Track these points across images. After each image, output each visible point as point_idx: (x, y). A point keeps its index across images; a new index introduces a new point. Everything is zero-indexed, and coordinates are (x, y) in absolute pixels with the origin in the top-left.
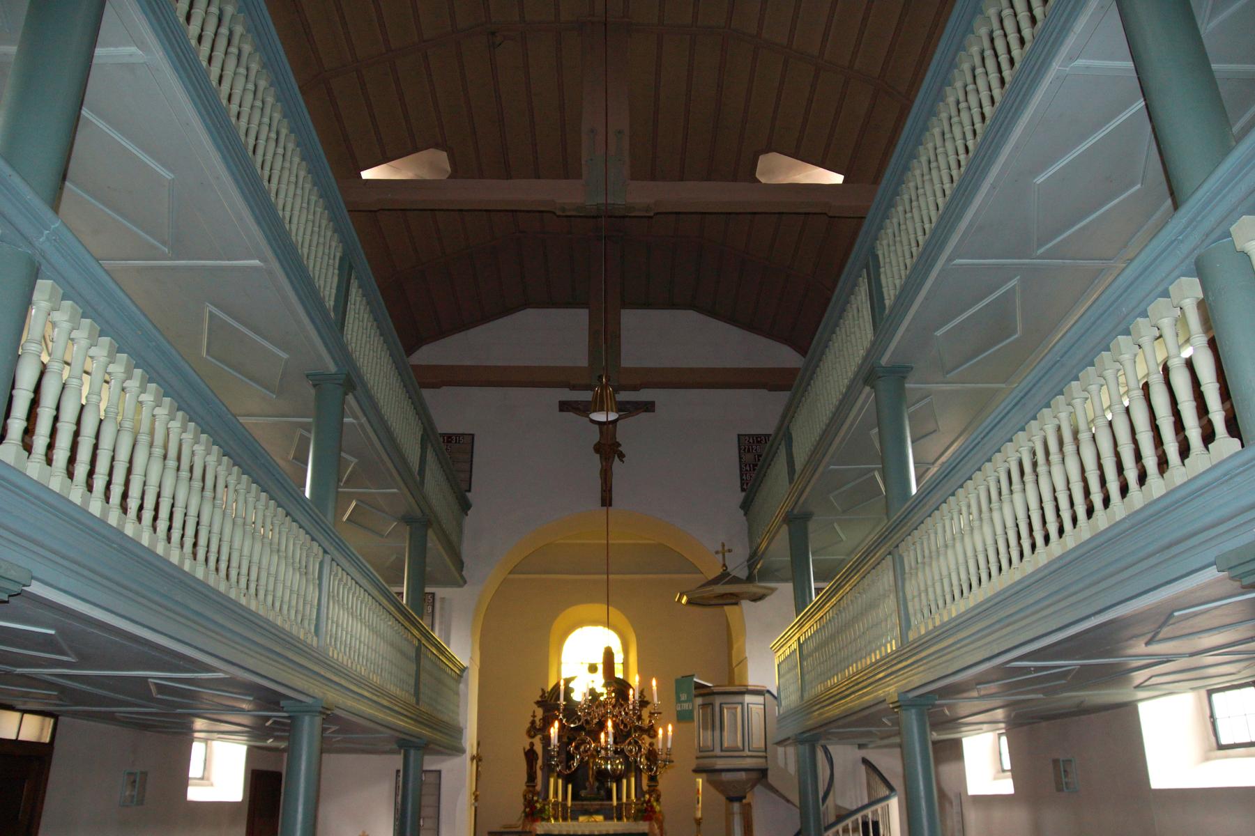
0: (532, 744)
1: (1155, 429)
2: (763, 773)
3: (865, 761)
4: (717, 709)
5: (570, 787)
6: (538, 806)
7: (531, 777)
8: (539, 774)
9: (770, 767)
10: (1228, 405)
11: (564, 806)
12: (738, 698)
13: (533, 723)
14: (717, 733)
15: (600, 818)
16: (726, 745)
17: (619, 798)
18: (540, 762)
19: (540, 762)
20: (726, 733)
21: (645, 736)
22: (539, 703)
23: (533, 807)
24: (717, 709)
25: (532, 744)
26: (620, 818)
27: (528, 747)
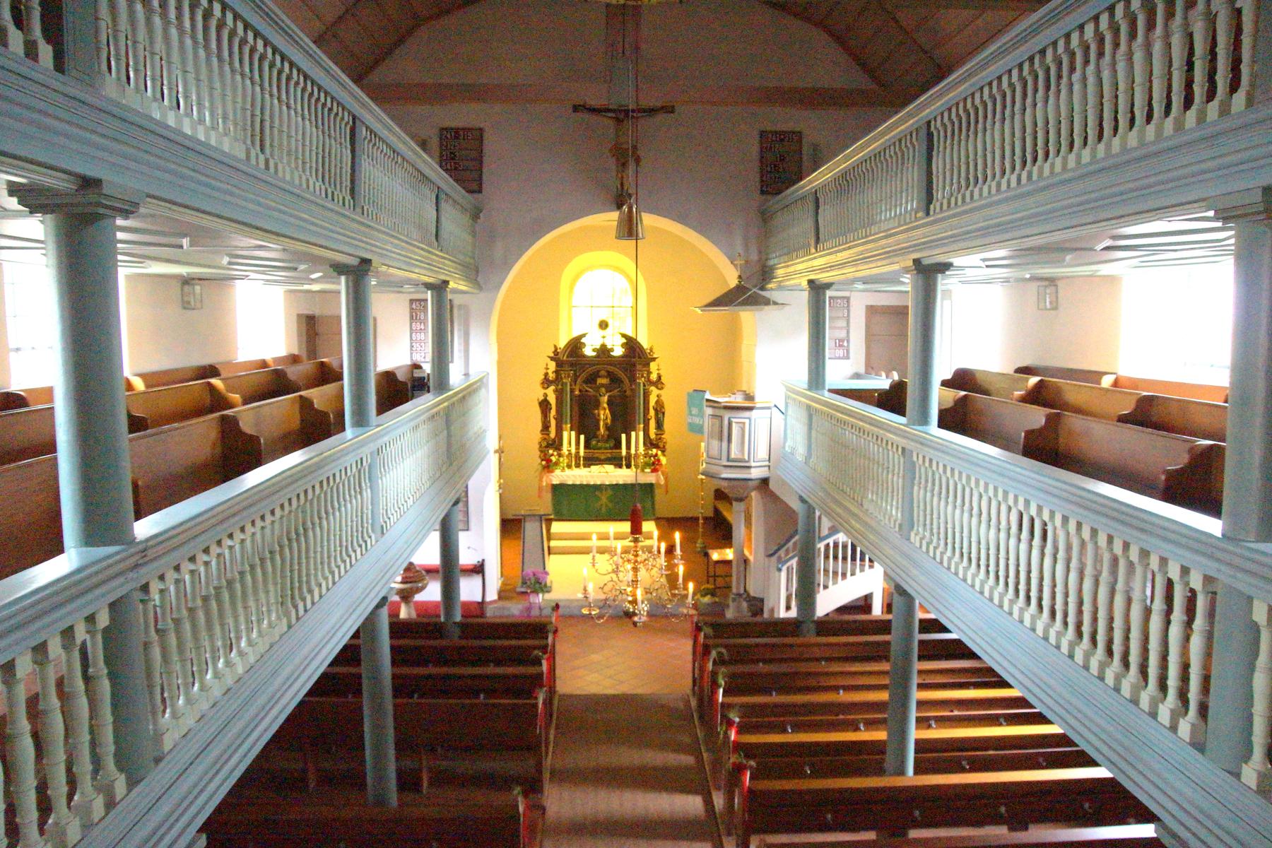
0: (546, 395)
1: (1018, 572)
2: (765, 481)
4: (726, 422)
5: (582, 437)
6: (554, 459)
7: (546, 427)
8: (553, 423)
9: (757, 195)
10: (1002, 720)
11: (577, 456)
12: (746, 414)
13: (546, 374)
14: (725, 444)
15: (610, 468)
16: (733, 456)
17: (628, 447)
18: (553, 412)
19: (553, 412)
20: (733, 445)
21: (653, 388)
22: (552, 359)
23: (549, 461)
24: (726, 422)
25: (546, 395)
26: (628, 466)
27: (542, 398)
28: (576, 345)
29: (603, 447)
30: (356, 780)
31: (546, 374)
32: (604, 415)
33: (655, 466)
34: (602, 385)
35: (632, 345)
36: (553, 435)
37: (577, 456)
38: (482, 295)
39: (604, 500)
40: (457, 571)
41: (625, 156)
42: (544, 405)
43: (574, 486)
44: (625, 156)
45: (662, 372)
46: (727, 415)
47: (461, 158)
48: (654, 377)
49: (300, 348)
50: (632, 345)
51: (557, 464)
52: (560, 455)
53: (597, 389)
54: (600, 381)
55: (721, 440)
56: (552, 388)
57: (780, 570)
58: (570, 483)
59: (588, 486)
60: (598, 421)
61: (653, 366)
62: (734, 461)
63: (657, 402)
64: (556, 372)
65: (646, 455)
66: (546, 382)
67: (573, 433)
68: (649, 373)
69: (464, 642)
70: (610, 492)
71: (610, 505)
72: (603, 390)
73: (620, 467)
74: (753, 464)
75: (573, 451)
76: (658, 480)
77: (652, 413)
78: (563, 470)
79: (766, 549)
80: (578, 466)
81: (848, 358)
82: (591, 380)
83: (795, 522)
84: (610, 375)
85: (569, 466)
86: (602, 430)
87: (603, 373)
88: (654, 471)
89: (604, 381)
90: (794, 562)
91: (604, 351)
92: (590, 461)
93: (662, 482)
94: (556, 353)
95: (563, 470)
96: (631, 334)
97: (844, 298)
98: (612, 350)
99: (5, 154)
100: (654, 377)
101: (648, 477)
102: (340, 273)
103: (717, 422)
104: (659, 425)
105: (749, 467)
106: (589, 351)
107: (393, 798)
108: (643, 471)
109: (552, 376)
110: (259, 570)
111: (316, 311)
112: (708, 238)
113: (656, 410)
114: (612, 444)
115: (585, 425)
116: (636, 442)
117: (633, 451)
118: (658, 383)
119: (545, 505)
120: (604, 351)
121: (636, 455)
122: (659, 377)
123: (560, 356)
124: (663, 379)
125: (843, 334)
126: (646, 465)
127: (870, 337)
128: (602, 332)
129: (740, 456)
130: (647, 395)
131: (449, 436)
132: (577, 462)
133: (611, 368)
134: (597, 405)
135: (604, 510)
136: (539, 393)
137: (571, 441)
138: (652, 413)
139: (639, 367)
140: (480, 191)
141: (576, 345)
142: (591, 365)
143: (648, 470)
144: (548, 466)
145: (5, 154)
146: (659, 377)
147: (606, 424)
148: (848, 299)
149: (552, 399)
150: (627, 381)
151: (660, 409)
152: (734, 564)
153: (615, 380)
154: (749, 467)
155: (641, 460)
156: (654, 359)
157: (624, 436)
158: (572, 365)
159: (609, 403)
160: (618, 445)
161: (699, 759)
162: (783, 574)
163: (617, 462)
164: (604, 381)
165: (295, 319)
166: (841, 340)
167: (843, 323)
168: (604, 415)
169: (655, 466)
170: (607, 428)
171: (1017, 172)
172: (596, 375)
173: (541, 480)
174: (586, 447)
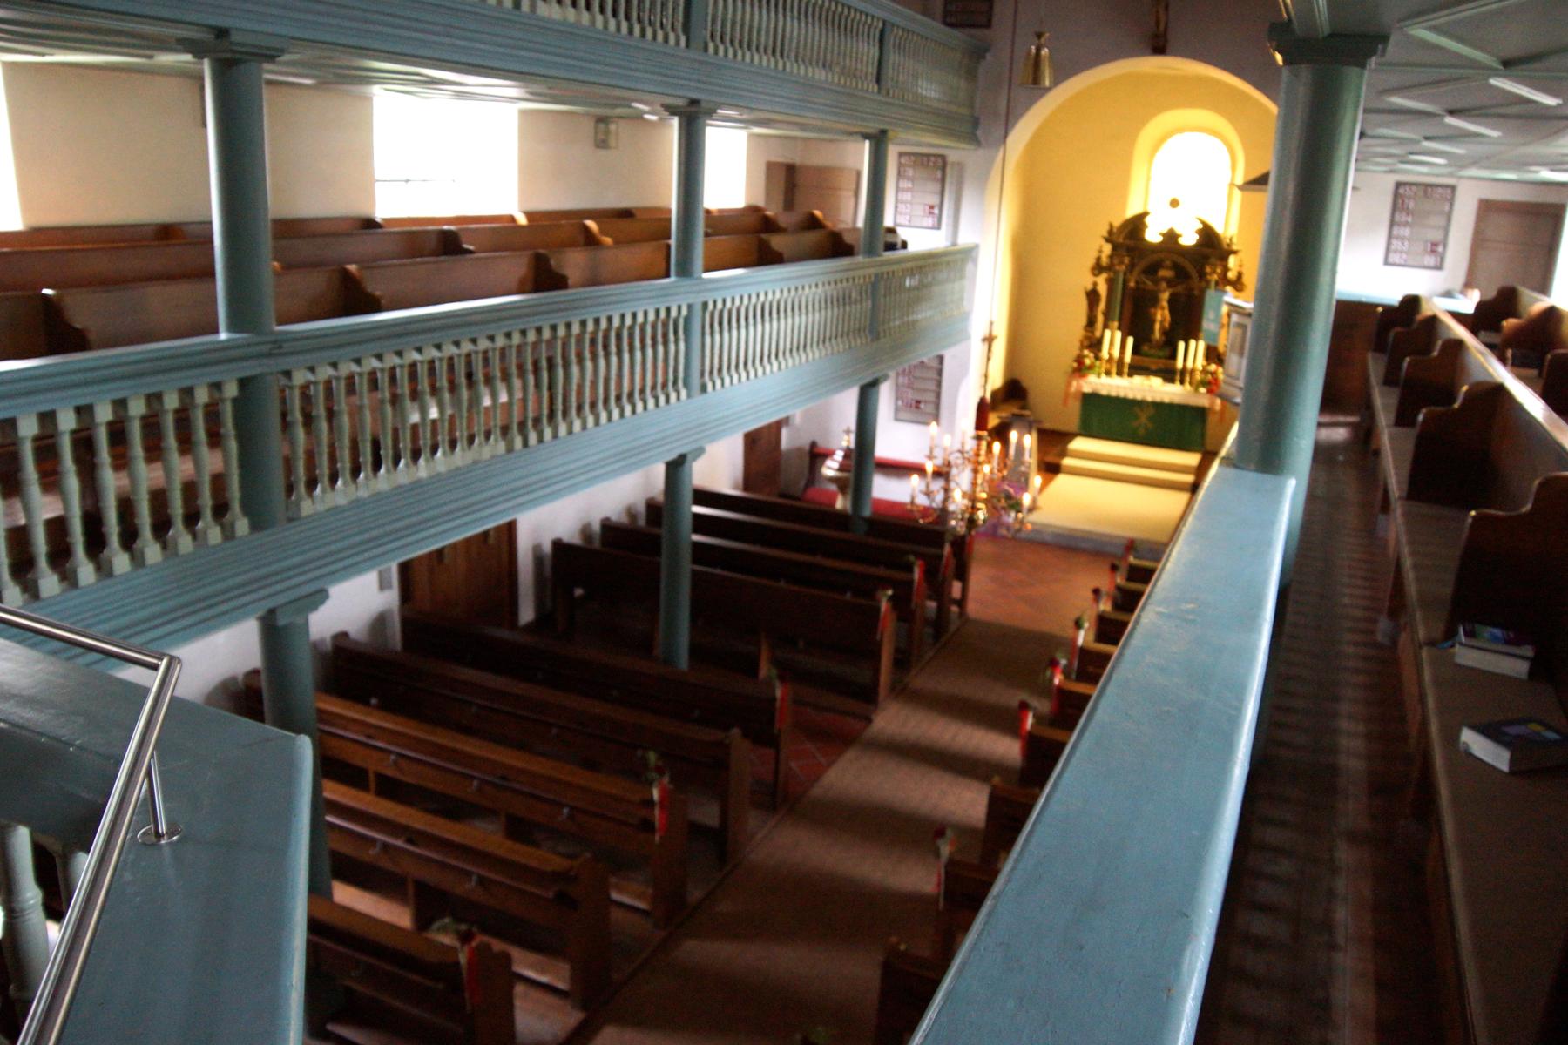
0: (1095, 284)
5: (1130, 341)
6: (1087, 362)
7: (1091, 323)
13: (1098, 259)
18: (1102, 306)
19: (1102, 306)
22: (1108, 240)
25: (1095, 284)
27: (1090, 287)
28: (1136, 225)
29: (1154, 356)
30: (645, 645)
32: (1162, 316)
34: (1164, 279)
35: (1208, 236)
38: (981, 152)
39: (1143, 419)
40: (871, 466)
42: (1092, 296)
49: (768, 195)
50: (1208, 236)
51: (1091, 368)
52: (1097, 358)
53: (1156, 282)
56: (1104, 276)
60: (1153, 322)
61: (1232, 261)
64: (1111, 257)
65: (1205, 371)
66: (1098, 268)
67: (1118, 335)
68: (1226, 269)
69: (871, 540)
72: (1164, 285)
75: (1116, 354)
76: (1213, 403)
78: (1099, 376)
80: (1120, 373)
81: (939, 227)
82: (1152, 270)
84: (1176, 267)
85: (1108, 373)
92: (1135, 370)
94: (1110, 232)
95: (1099, 376)
97: (1447, 186)
100: (1231, 275)
101: (1202, 399)
102: (673, 114)
103: (1239, 331)
106: (1153, 235)
107: (683, 661)
108: (1196, 390)
109: (1105, 261)
110: (531, 415)
111: (797, 159)
114: (1167, 352)
115: (1136, 323)
116: (1192, 354)
119: (1070, 417)
120: (1171, 237)
122: (1240, 275)
123: (1114, 238)
125: (1436, 235)
126: (1203, 383)
127: (1479, 242)
131: (875, 309)
133: (1180, 260)
134: (1155, 301)
136: (1087, 281)
137: (1114, 342)
139: (1212, 260)
140: (988, 25)
141: (1136, 225)
143: (1203, 390)
144: (1080, 369)
146: (1240, 275)
148: (1453, 188)
149: (1103, 289)
150: (1195, 275)
153: (1181, 274)
155: (1198, 376)
156: (1235, 252)
159: (1170, 301)
160: (1174, 356)
163: (1169, 375)
165: (762, 169)
166: (1435, 245)
167: (1441, 221)
168: (1162, 316)
170: (1164, 332)
173: (1069, 384)
174: (1136, 351)
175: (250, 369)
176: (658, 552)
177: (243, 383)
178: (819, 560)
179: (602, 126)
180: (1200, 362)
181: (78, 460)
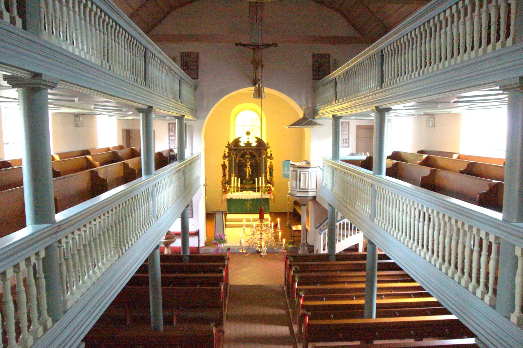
0: (224, 162)
1: (418, 235)
2: (314, 198)
3: (341, 160)
4: (298, 173)
5: (239, 179)
6: (228, 188)
7: (224, 175)
8: (227, 173)
9: (311, 80)
10: (412, 295)
11: (237, 187)
12: (307, 170)
13: (225, 154)
14: (298, 182)
15: (251, 192)
16: (301, 187)
17: (258, 184)
18: (227, 169)
19: (227, 169)
20: (302, 183)
21: (268, 159)
22: (227, 147)
23: (226, 189)
24: (298, 173)
25: (224, 162)
26: (258, 191)
27: (223, 163)
28: (237, 142)
29: (248, 183)
31: (225, 154)
32: (248, 170)
33: (269, 191)
34: (248, 158)
35: (260, 142)
36: (227, 178)
37: (237, 187)
38: (198, 121)
39: (248, 205)
40: (188, 234)
41: (257, 64)
42: (224, 166)
43: (236, 199)
44: (257, 64)
45: (272, 153)
46: (299, 170)
47: (190, 65)
48: (269, 155)
49: (123, 143)
50: (260, 142)
51: (229, 190)
52: (230, 187)
53: (246, 160)
54: (247, 156)
55: (297, 181)
56: (227, 159)
57: (321, 234)
58: (234, 198)
59: (242, 199)
60: (246, 173)
61: (268, 150)
62: (302, 189)
63: (270, 165)
64: (229, 153)
65: (266, 187)
66: (225, 157)
67: (236, 178)
68: (267, 153)
69: (191, 264)
70: (251, 202)
71: (251, 207)
72: (248, 160)
73: (255, 192)
74: (310, 190)
75: (236, 185)
76: (270, 197)
77: (268, 169)
78: (232, 193)
79: (315, 225)
80: (237, 191)
81: (349, 147)
82: (243, 156)
83: (327, 214)
84: (251, 154)
85: (234, 191)
86: (248, 177)
87: (248, 153)
88: (269, 193)
89: (248, 156)
90: (326, 231)
91: (248, 144)
92: (242, 189)
93: (272, 198)
94: (229, 145)
95: (232, 193)
96: (259, 137)
97: (347, 122)
98: (252, 144)
99: (2, 63)
100: (269, 155)
101: (266, 196)
102: (140, 112)
103: (295, 173)
104: (271, 175)
105: (308, 192)
106: (242, 144)
107: (162, 327)
108: (264, 193)
109: (227, 154)
111: (130, 128)
112: (291, 98)
113: (270, 168)
114: (251, 182)
115: (241, 174)
116: (261, 181)
117: (260, 185)
118: (271, 157)
119: (224, 207)
120: (248, 144)
121: (262, 187)
122: (271, 155)
123: (230, 146)
124: (273, 156)
125: (347, 137)
126: (266, 191)
127: (358, 138)
128: (248, 136)
129: (304, 187)
130: (266, 162)
131: (185, 179)
132: (237, 189)
133: (251, 151)
134: (246, 166)
135: (248, 209)
136: (222, 161)
137: (235, 181)
138: (268, 169)
139: (263, 151)
140: (197, 79)
141: (237, 142)
142: (243, 150)
143: (266, 193)
144: (225, 191)
145: (2, 63)
146: (271, 155)
147: (249, 174)
148: (349, 123)
149: (227, 164)
150: (258, 156)
151: (271, 168)
152: (302, 232)
153: (253, 156)
154: (308, 192)
155: (264, 189)
156: (269, 147)
157: (256, 179)
158: (235, 150)
159: (250, 165)
160: (254, 183)
161: (288, 311)
162: (322, 236)
163: (254, 190)
164: (248, 156)
165: (121, 131)
166: (346, 140)
167: (346, 133)
168: (248, 170)
169: (269, 191)
170: (250, 176)
171: (418, 70)
172: (245, 154)
173: (222, 197)
174: (241, 183)
175: (48, 242)
176: (147, 284)
177: (46, 249)
178: (202, 275)
179: (77, 118)
180: (264, 184)
181: (343, 317)
